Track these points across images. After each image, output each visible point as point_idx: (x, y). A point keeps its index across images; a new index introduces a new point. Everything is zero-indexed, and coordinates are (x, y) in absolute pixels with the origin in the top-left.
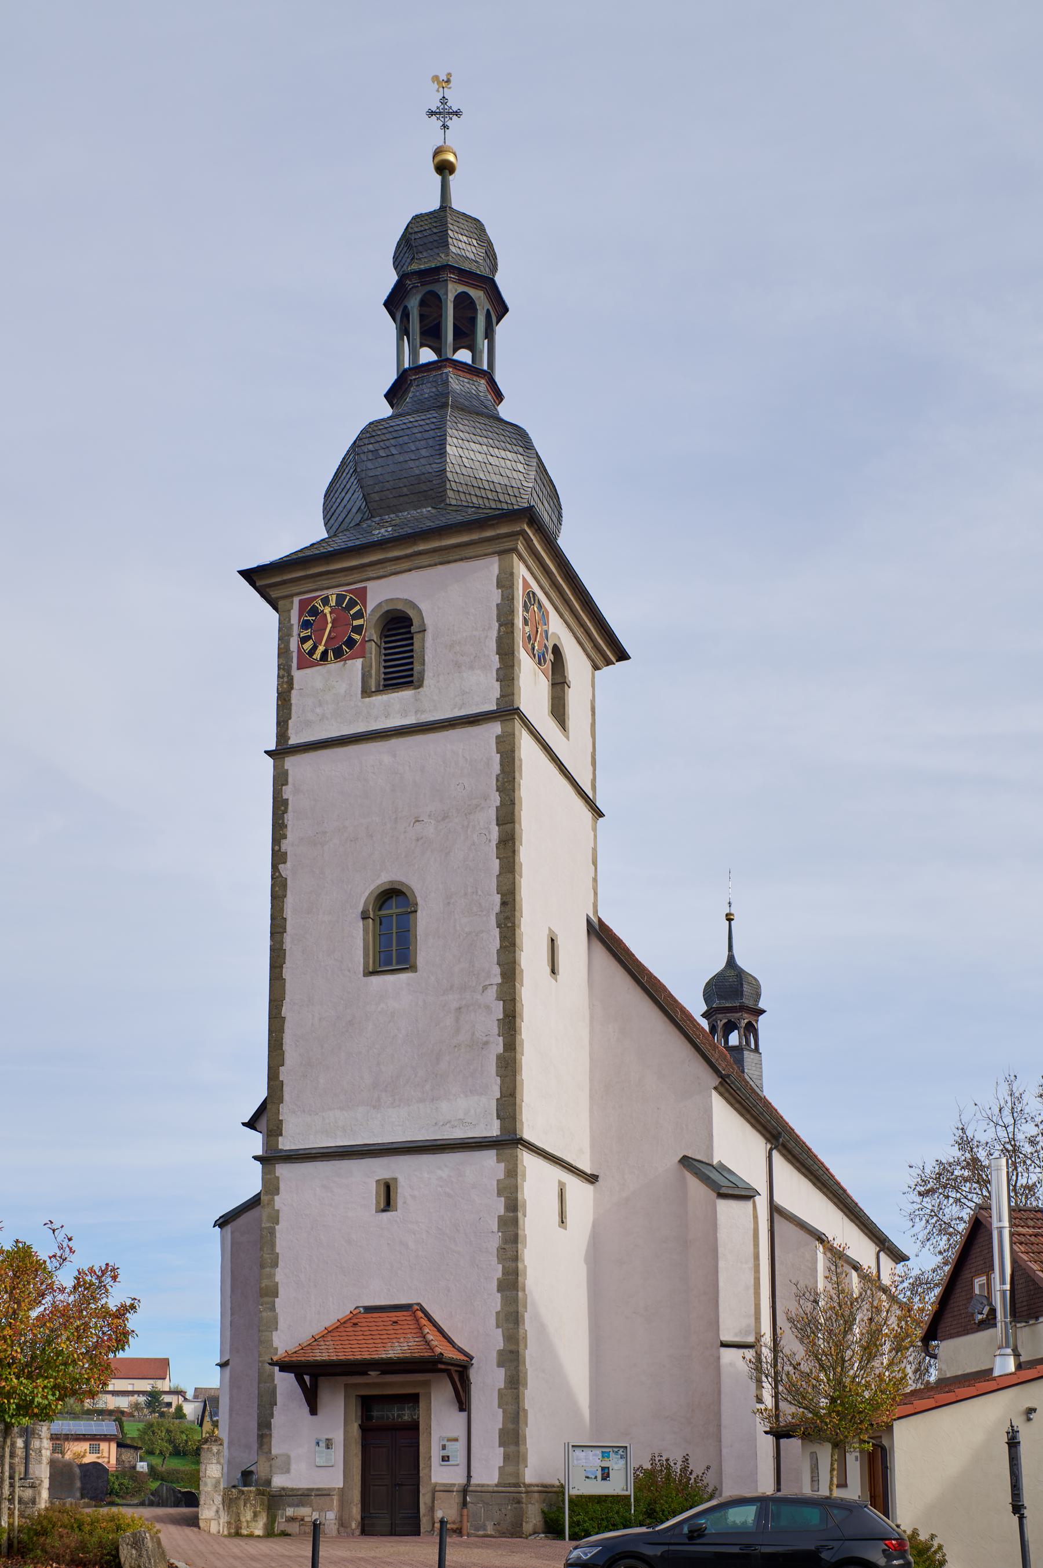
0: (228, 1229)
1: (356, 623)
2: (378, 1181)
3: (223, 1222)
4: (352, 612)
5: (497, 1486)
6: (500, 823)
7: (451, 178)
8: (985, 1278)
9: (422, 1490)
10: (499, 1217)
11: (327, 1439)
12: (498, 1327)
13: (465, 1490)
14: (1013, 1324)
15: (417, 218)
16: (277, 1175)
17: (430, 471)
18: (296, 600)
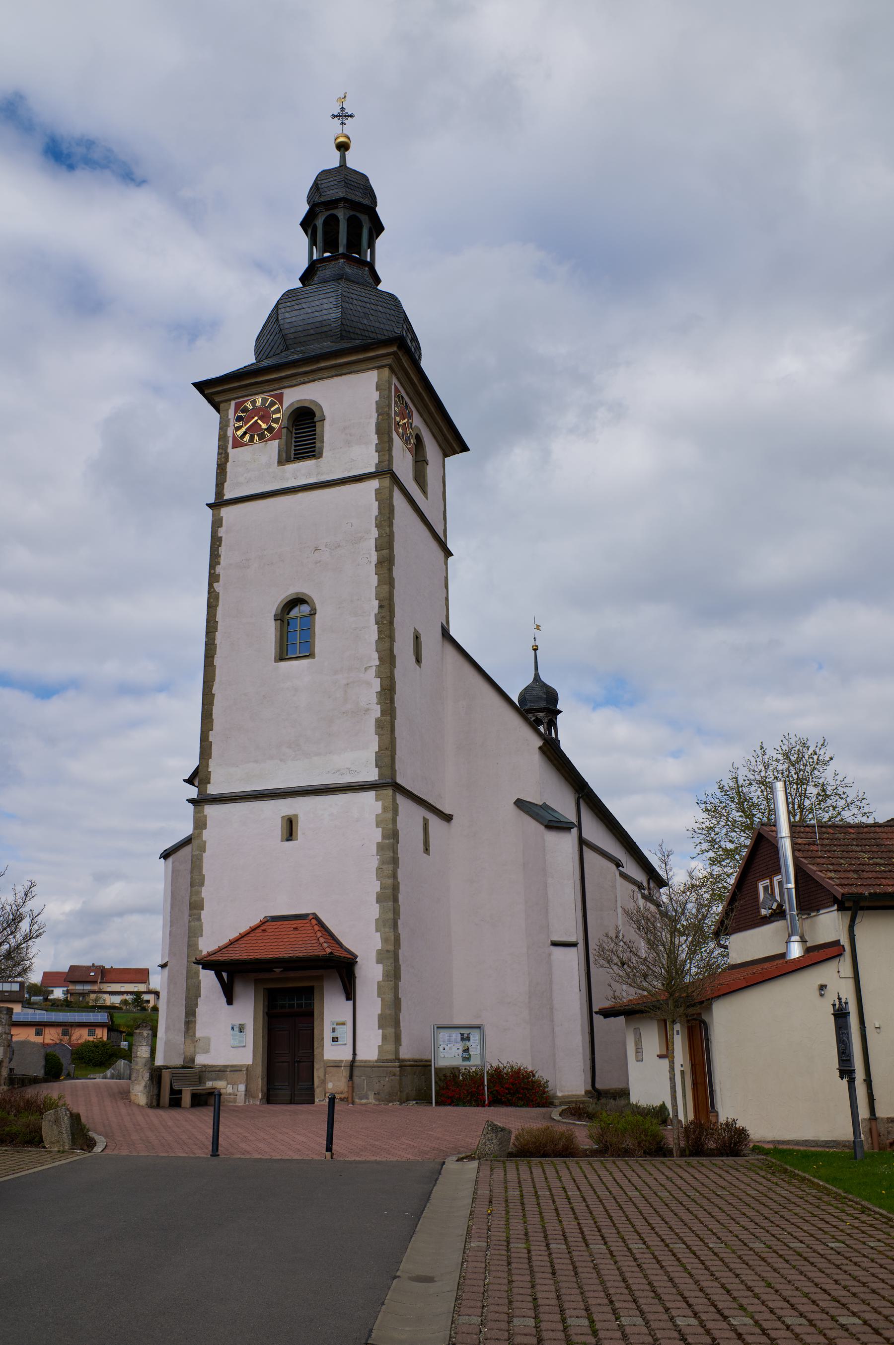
0: (170, 860)
1: (274, 416)
2: (283, 817)
3: (166, 855)
4: (272, 409)
5: (376, 1061)
6: (379, 549)
7: (346, 153)
8: (768, 881)
9: (316, 1066)
10: (378, 843)
11: (240, 1025)
12: (377, 931)
13: (352, 1065)
14: (800, 916)
15: (324, 172)
16: (205, 814)
17: (330, 318)
18: (233, 403)
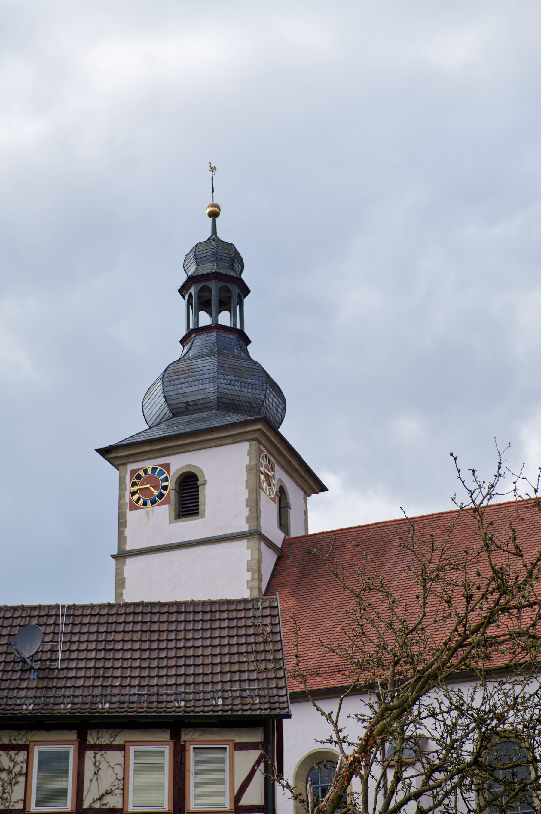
4: (161, 478)
10: (246, 465)
